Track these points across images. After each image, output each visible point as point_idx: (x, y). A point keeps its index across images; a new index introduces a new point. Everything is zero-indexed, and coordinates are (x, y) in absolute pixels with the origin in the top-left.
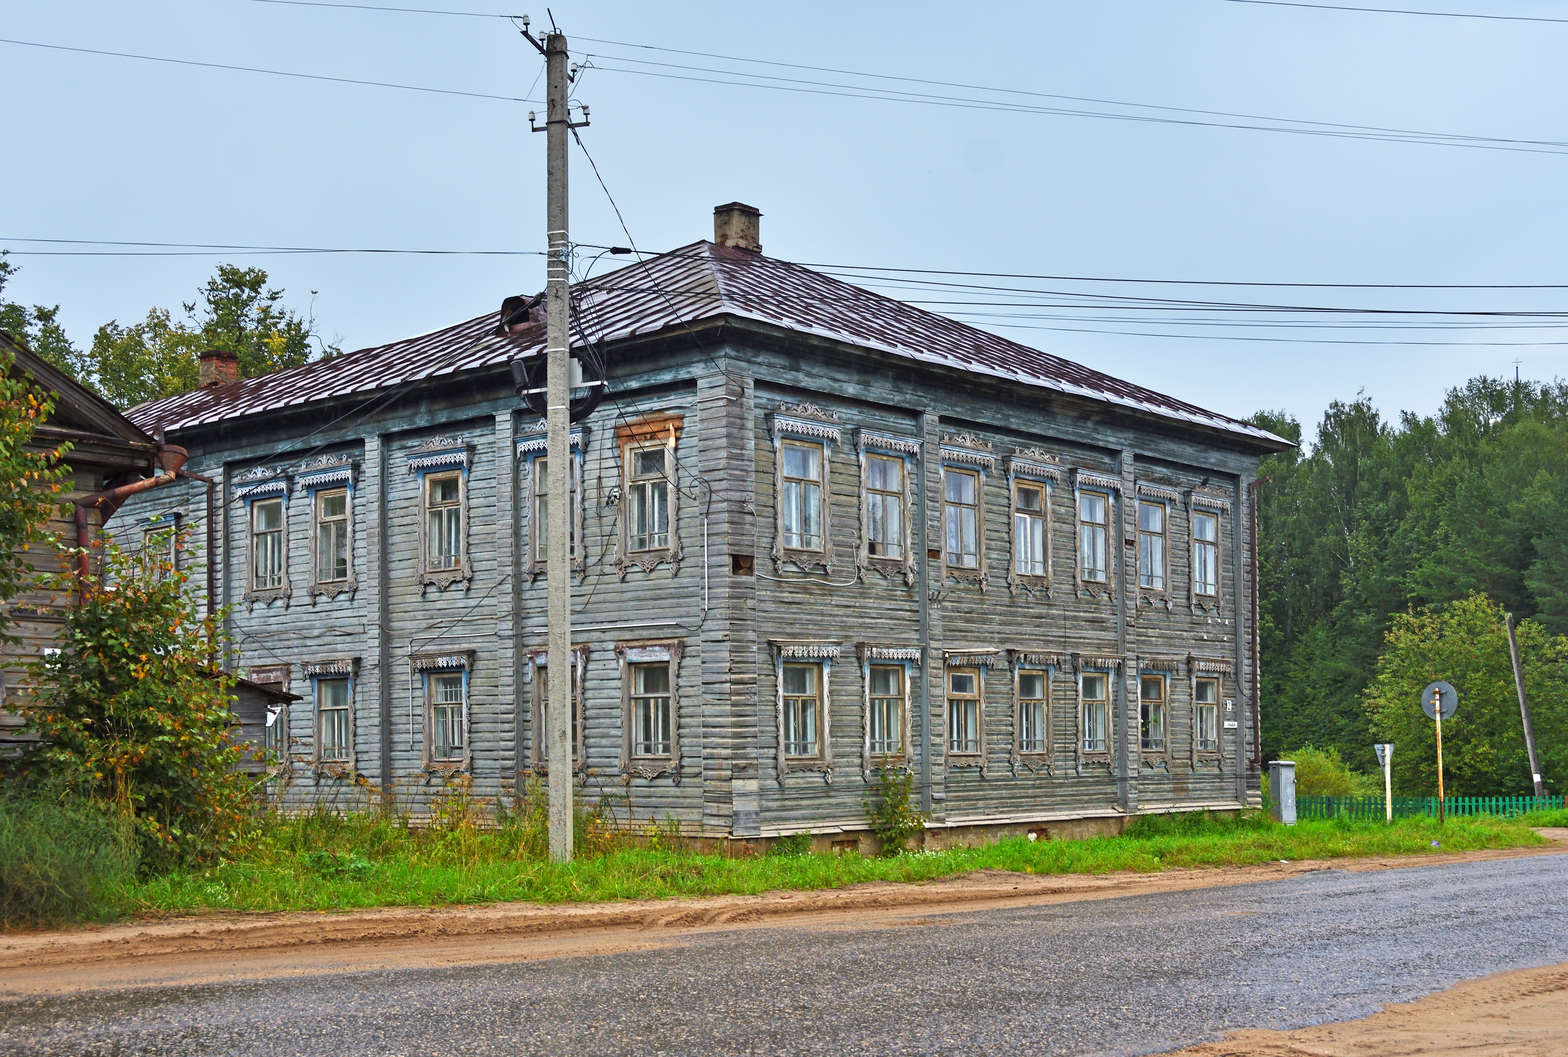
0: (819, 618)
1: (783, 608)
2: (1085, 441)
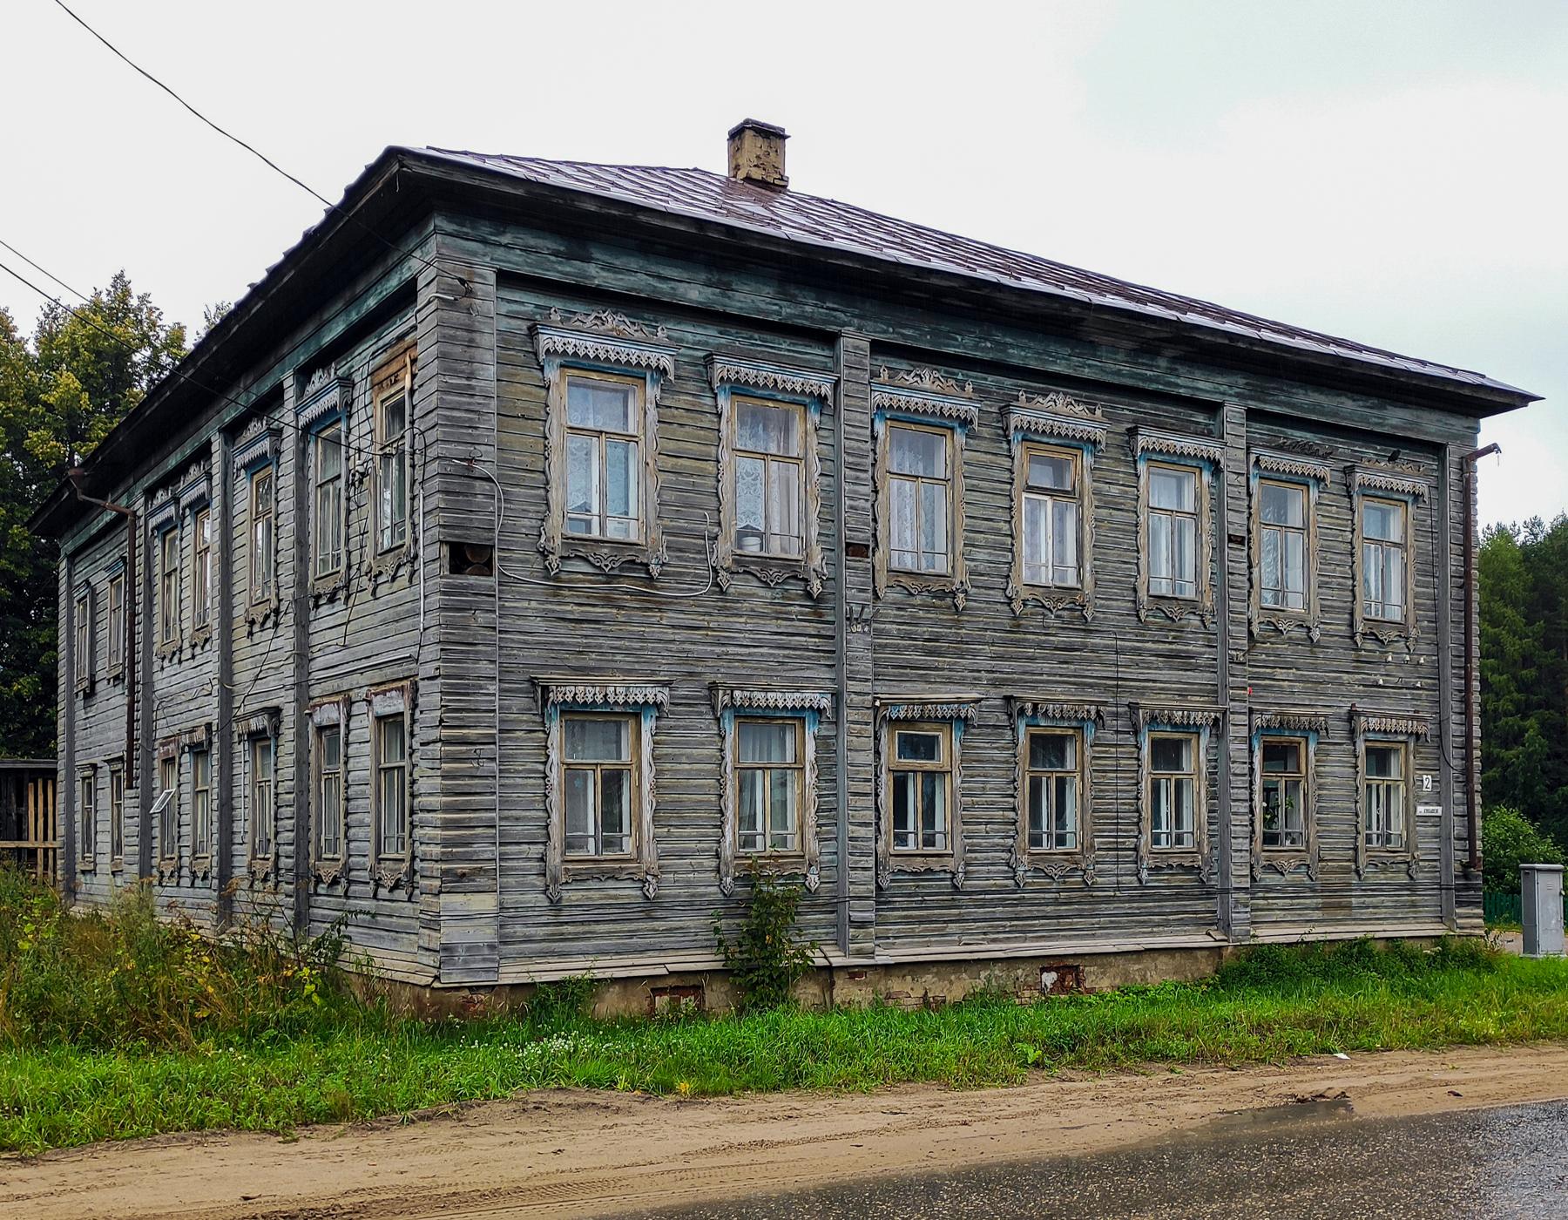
0: (637, 645)
1: (563, 628)
2: (1154, 386)
